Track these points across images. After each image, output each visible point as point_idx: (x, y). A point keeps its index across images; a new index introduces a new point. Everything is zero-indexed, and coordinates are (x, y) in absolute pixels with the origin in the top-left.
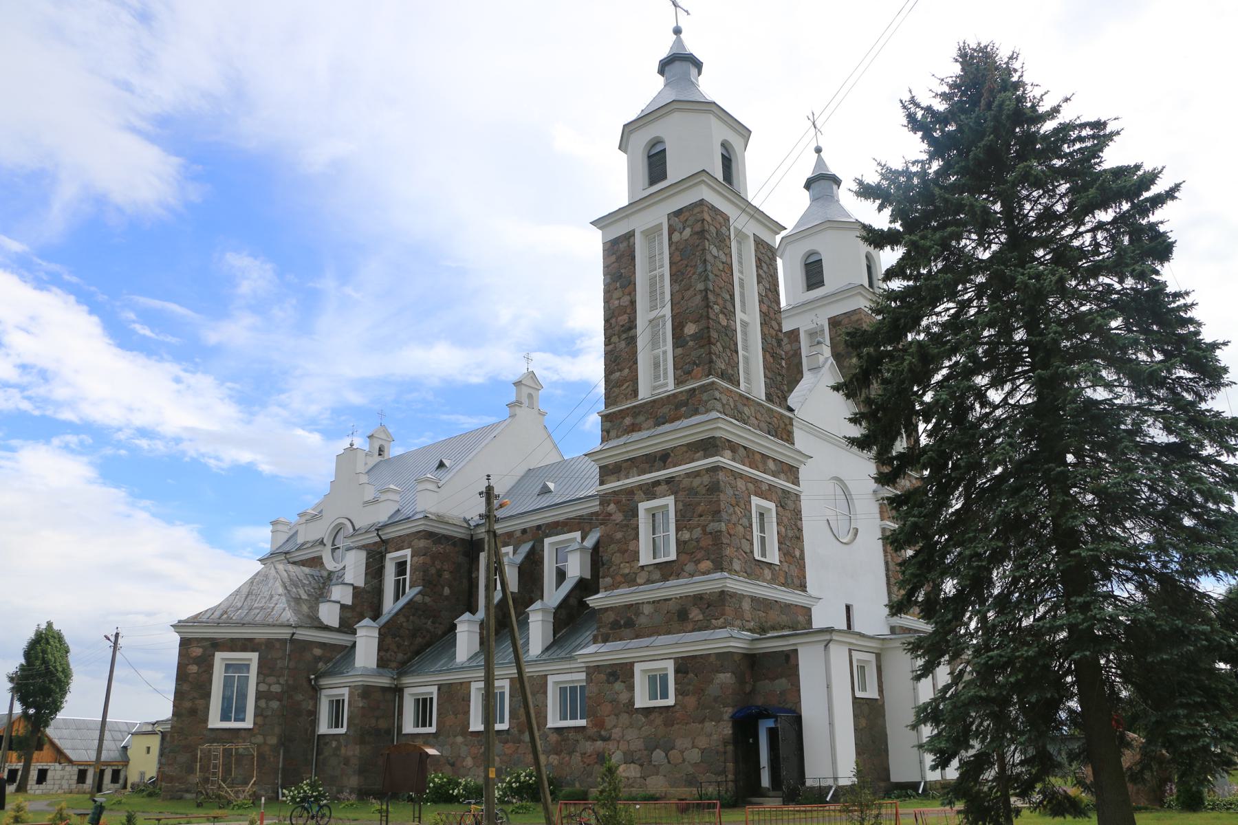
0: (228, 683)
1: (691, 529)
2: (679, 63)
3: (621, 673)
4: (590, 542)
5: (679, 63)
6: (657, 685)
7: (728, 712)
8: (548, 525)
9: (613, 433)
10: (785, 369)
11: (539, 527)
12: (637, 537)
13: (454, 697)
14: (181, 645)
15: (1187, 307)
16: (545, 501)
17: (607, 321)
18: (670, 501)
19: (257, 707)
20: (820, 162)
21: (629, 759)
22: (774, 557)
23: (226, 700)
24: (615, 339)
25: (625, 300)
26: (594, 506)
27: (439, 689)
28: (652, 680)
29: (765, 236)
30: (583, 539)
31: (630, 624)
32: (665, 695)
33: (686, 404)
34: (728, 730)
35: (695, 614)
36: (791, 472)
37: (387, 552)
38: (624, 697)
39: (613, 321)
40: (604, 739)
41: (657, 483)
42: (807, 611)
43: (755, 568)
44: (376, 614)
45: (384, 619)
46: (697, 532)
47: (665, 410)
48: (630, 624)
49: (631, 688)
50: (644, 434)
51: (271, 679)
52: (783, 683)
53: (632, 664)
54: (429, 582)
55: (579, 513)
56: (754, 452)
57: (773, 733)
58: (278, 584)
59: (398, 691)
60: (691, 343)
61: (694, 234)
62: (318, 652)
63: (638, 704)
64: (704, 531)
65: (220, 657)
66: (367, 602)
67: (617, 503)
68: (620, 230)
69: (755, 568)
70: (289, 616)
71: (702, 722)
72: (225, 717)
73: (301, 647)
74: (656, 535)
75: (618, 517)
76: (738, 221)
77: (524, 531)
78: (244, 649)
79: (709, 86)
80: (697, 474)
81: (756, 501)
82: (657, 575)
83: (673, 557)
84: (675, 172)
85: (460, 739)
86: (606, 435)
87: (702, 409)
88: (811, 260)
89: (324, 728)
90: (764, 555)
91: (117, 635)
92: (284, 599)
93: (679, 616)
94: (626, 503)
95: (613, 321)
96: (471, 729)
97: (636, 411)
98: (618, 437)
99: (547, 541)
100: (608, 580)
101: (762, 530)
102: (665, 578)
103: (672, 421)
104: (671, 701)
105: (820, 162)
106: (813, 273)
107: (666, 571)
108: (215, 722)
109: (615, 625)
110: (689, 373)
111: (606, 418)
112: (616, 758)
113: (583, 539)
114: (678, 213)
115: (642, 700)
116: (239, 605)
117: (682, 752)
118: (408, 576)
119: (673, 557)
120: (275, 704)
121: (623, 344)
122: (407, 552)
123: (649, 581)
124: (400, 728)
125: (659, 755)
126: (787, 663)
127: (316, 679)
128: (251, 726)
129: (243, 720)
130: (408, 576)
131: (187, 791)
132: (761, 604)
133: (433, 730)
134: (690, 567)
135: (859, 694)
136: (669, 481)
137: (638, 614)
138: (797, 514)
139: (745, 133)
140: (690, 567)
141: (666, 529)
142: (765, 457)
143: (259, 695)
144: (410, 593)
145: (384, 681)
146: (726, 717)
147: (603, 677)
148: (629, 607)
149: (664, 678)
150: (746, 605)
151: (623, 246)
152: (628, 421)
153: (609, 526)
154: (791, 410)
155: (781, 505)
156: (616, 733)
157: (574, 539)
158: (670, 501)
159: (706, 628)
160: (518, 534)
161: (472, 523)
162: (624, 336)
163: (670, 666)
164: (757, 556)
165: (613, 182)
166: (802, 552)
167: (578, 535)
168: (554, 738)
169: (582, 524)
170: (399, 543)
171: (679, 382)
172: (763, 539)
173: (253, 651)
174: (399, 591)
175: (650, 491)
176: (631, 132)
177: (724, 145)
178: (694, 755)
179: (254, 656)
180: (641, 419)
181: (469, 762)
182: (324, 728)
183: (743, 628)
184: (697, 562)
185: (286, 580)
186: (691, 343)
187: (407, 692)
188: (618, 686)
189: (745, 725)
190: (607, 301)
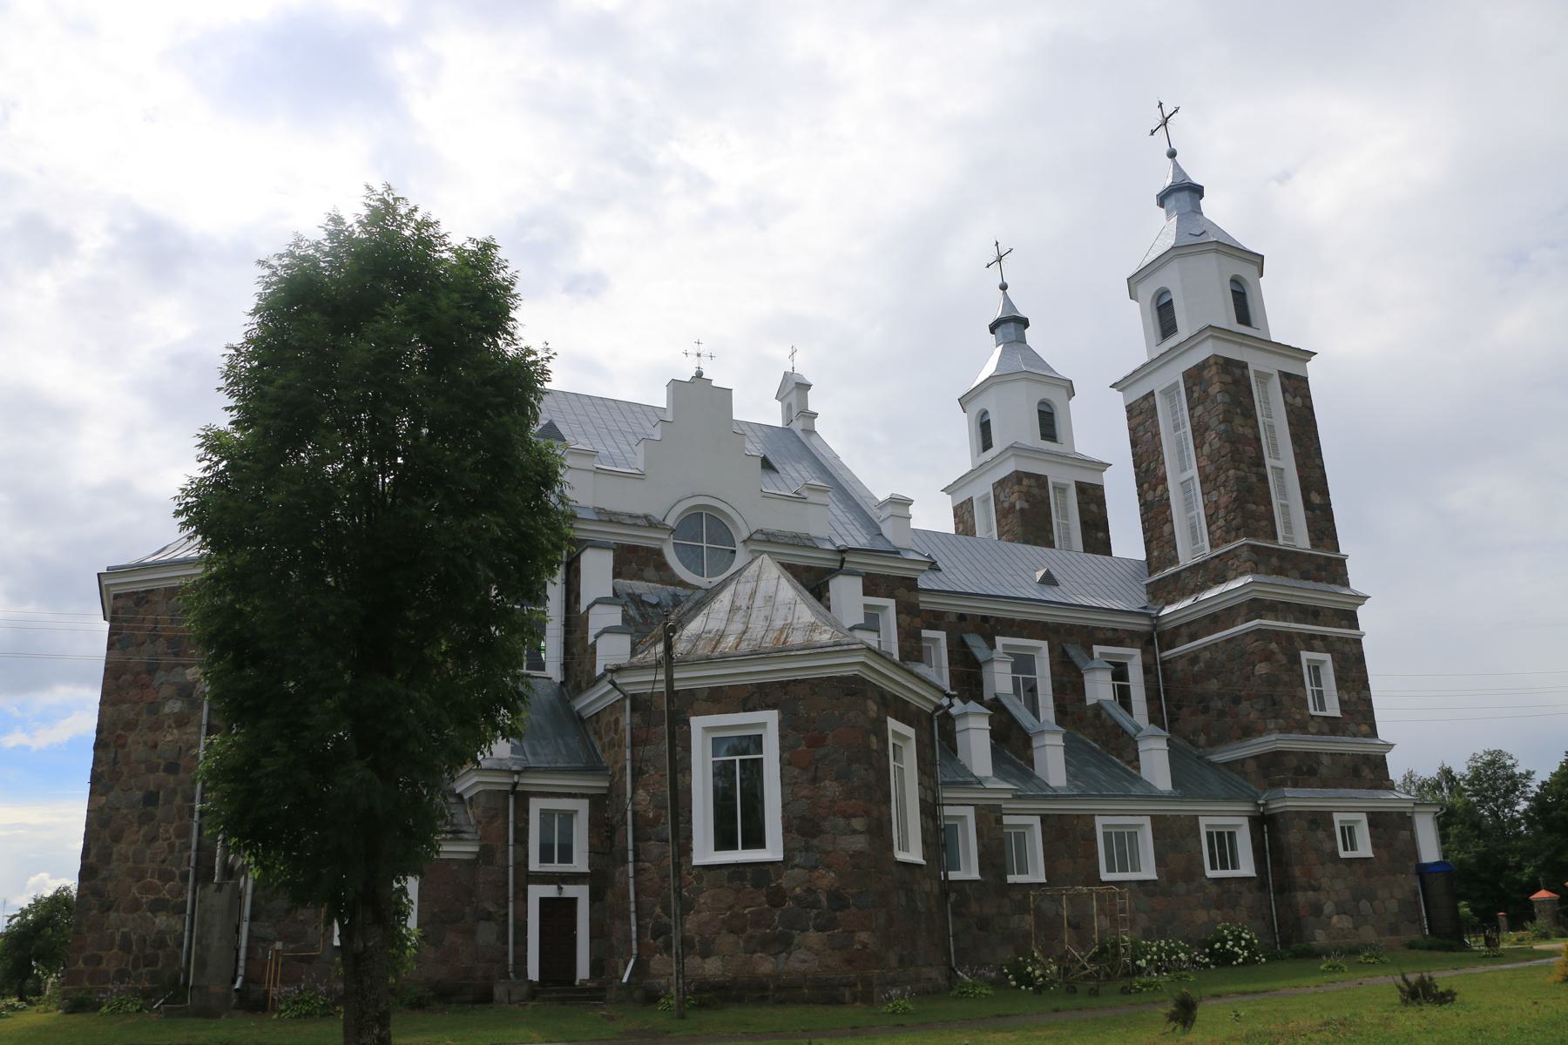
0: (723, 772)
16: (1050, 594)
20: (1008, 302)
21: (1341, 910)
27: (1042, 822)
31: (1312, 772)
36: (1351, 619)
40: (1315, 889)
53: (1330, 813)
55: (1061, 620)
72: (724, 840)
76: (1256, 362)
78: (746, 707)
81: (1305, 656)
82: (1326, 728)
84: (1184, 330)
90: (1323, 708)
99: (1044, 644)
102: (1333, 732)
104: (773, 851)
105: (1008, 302)
108: (704, 852)
109: (1298, 771)
112: (1328, 908)
125: (1364, 905)
137: (1319, 763)
139: (1257, 261)
140: (1352, 727)
177: (1236, 281)
178: (1393, 906)
179: (769, 719)
184: (1358, 725)
188: (1321, 834)
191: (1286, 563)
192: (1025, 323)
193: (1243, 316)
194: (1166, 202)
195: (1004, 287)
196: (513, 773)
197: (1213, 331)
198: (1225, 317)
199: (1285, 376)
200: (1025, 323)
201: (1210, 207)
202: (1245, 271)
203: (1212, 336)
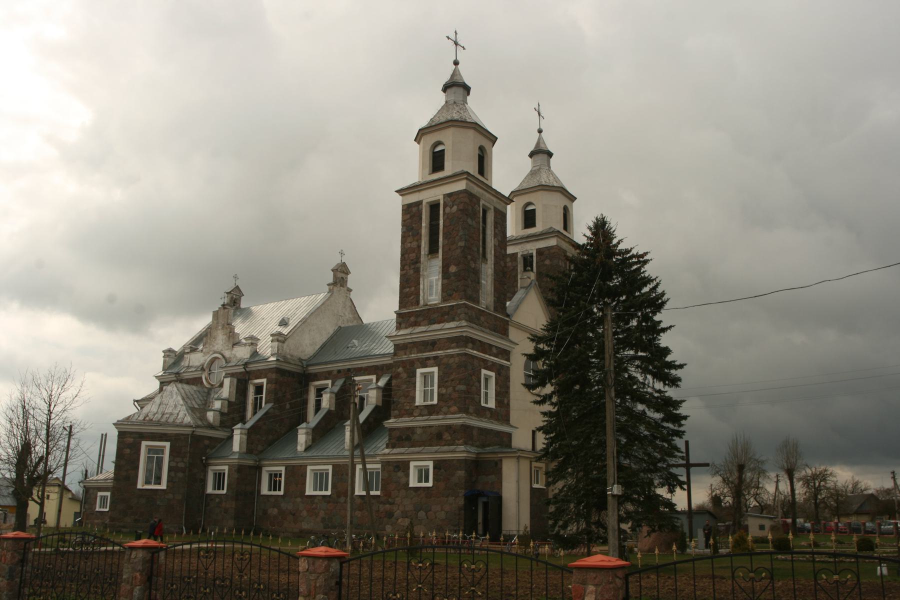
0: (149, 460)
1: (447, 387)
2: (456, 87)
3: (403, 467)
4: (382, 383)
5: (456, 87)
6: (423, 475)
7: (462, 492)
8: (355, 369)
9: (403, 325)
10: (505, 286)
11: (349, 370)
12: (415, 389)
13: (296, 475)
14: (119, 436)
15: (663, 294)
17: (402, 255)
18: (435, 370)
19: (169, 476)
22: (492, 404)
23: (148, 471)
24: (407, 267)
25: (415, 244)
26: (388, 361)
28: (420, 472)
29: (500, 207)
30: (378, 380)
31: (408, 439)
32: (427, 481)
33: (448, 314)
34: (461, 502)
35: (447, 436)
37: (249, 379)
38: (403, 480)
39: (406, 256)
40: (390, 504)
41: (428, 358)
42: (509, 435)
43: (482, 412)
44: (243, 420)
45: (248, 425)
46: (450, 390)
47: (435, 316)
48: (408, 439)
49: (408, 475)
50: (422, 328)
51: (178, 459)
52: (492, 478)
53: (409, 462)
54: (276, 397)
56: (485, 343)
57: (486, 505)
58: (179, 398)
59: (258, 469)
60: (453, 278)
61: (459, 210)
62: (207, 442)
63: (411, 485)
64: (454, 390)
65: (144, 444)
66: (234, 412)
67: (404, 367)
68: (413, 198)
69: (482, 412)
70: (188, 419)
71: (447, 497)
73: (196, 439)
74: (426, 386)
75: (404, 376)
77: (339, 371)
79: (478, 108)
80: (452, 356)
82: (426, 412)
83: (435, 402)
85: (299, 500)
86: (399, 327)
87: (457, 318)
88: (530, 208)
89: (210, 490)
90: (486, 402)
91: (71, 427)
92: (184, 408)
93: (437, 437)
94: (410, 368)
95: (406, 256)
96: (307, 494)
97: (417, 314)
98: (406, 328)
100: (396, 412)
101: (486, 387)
102: (430, 414)
103: (439, 323)
104: (430, 484)
106: (529, 219)
107: (431, 410)
110: (450, 295)
111: (399, 315)
112: (397, 513)
113: (378, 380)
114: (450, 195)
115: (413, 483)
116: (155, 410)
117: (435, 513)
118: (264, 396)
119: (435, 402)
120: (180, 475)
121: (412, 272)
122: (264, 381)
123: (421, 415)
124: (259, 491)
125: (422, 514)
126: (496, 468)
127: (206, 460)
128: (165, 488)
129: (160, 484)
130: (264, 396)
131: (124, 527)
132: (482, 430)
133: (282, 493)
134: (445, 409)
135: (535, 486)
136: (436, 358)
138: (507, 379)
139: (493, 139)
141: (432, 385)
142: (491, 346)
143: (170, 469)
144: (266, 407)
145: (250, 462)
146: (460, 495)
147: (391, 468)
148: (408, 428)
149: (427, 471)
150: (475, 433)
151: (414, 209)
152: (412, 319)
153: (398, 374)
154: (508, 316)
155: (498, 374)
156: (398, 500)
157: (371, 380)
158: (435, 370)
159: (453, 445)
160: (335, 373)
161: (304, 363)
162: (412, 267)
163: (430, 464)
164: (483, 404)
165: (411, 167)
166: (509, 401)
167: (374, 377)
168: (359, 501)
169: (378, 370)
170: (259, 374)
171: (444, 299)
172: (486, 394)
173: (167, 441)
174: (257, 406)
175: (424, 363)
176: (423, 134)
177: (481, 149)
178: (442, 515)
179: (167, 445)
180: (420, 319)
181: (305, 513)
182: (210, 490)
183: (472, 445)
184: (449, 407)
185: (184, 395)
186: (453, 278)
187: (265, 469)
188: (400, 474)
189: (472, 499)
190: (403, 242)
191: (476, 318)
192: (550, 155)
193: (481, 171)
194: (449, 90)
195: (540, 131)
196: (191, 426)
197: (466, 175)
198: (472, 168)
199: (497, 211)
200: (550, 155)
201: (472, 101)
202: (485, 143)
203: (466, 178)
